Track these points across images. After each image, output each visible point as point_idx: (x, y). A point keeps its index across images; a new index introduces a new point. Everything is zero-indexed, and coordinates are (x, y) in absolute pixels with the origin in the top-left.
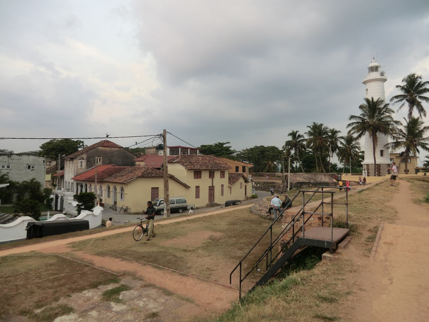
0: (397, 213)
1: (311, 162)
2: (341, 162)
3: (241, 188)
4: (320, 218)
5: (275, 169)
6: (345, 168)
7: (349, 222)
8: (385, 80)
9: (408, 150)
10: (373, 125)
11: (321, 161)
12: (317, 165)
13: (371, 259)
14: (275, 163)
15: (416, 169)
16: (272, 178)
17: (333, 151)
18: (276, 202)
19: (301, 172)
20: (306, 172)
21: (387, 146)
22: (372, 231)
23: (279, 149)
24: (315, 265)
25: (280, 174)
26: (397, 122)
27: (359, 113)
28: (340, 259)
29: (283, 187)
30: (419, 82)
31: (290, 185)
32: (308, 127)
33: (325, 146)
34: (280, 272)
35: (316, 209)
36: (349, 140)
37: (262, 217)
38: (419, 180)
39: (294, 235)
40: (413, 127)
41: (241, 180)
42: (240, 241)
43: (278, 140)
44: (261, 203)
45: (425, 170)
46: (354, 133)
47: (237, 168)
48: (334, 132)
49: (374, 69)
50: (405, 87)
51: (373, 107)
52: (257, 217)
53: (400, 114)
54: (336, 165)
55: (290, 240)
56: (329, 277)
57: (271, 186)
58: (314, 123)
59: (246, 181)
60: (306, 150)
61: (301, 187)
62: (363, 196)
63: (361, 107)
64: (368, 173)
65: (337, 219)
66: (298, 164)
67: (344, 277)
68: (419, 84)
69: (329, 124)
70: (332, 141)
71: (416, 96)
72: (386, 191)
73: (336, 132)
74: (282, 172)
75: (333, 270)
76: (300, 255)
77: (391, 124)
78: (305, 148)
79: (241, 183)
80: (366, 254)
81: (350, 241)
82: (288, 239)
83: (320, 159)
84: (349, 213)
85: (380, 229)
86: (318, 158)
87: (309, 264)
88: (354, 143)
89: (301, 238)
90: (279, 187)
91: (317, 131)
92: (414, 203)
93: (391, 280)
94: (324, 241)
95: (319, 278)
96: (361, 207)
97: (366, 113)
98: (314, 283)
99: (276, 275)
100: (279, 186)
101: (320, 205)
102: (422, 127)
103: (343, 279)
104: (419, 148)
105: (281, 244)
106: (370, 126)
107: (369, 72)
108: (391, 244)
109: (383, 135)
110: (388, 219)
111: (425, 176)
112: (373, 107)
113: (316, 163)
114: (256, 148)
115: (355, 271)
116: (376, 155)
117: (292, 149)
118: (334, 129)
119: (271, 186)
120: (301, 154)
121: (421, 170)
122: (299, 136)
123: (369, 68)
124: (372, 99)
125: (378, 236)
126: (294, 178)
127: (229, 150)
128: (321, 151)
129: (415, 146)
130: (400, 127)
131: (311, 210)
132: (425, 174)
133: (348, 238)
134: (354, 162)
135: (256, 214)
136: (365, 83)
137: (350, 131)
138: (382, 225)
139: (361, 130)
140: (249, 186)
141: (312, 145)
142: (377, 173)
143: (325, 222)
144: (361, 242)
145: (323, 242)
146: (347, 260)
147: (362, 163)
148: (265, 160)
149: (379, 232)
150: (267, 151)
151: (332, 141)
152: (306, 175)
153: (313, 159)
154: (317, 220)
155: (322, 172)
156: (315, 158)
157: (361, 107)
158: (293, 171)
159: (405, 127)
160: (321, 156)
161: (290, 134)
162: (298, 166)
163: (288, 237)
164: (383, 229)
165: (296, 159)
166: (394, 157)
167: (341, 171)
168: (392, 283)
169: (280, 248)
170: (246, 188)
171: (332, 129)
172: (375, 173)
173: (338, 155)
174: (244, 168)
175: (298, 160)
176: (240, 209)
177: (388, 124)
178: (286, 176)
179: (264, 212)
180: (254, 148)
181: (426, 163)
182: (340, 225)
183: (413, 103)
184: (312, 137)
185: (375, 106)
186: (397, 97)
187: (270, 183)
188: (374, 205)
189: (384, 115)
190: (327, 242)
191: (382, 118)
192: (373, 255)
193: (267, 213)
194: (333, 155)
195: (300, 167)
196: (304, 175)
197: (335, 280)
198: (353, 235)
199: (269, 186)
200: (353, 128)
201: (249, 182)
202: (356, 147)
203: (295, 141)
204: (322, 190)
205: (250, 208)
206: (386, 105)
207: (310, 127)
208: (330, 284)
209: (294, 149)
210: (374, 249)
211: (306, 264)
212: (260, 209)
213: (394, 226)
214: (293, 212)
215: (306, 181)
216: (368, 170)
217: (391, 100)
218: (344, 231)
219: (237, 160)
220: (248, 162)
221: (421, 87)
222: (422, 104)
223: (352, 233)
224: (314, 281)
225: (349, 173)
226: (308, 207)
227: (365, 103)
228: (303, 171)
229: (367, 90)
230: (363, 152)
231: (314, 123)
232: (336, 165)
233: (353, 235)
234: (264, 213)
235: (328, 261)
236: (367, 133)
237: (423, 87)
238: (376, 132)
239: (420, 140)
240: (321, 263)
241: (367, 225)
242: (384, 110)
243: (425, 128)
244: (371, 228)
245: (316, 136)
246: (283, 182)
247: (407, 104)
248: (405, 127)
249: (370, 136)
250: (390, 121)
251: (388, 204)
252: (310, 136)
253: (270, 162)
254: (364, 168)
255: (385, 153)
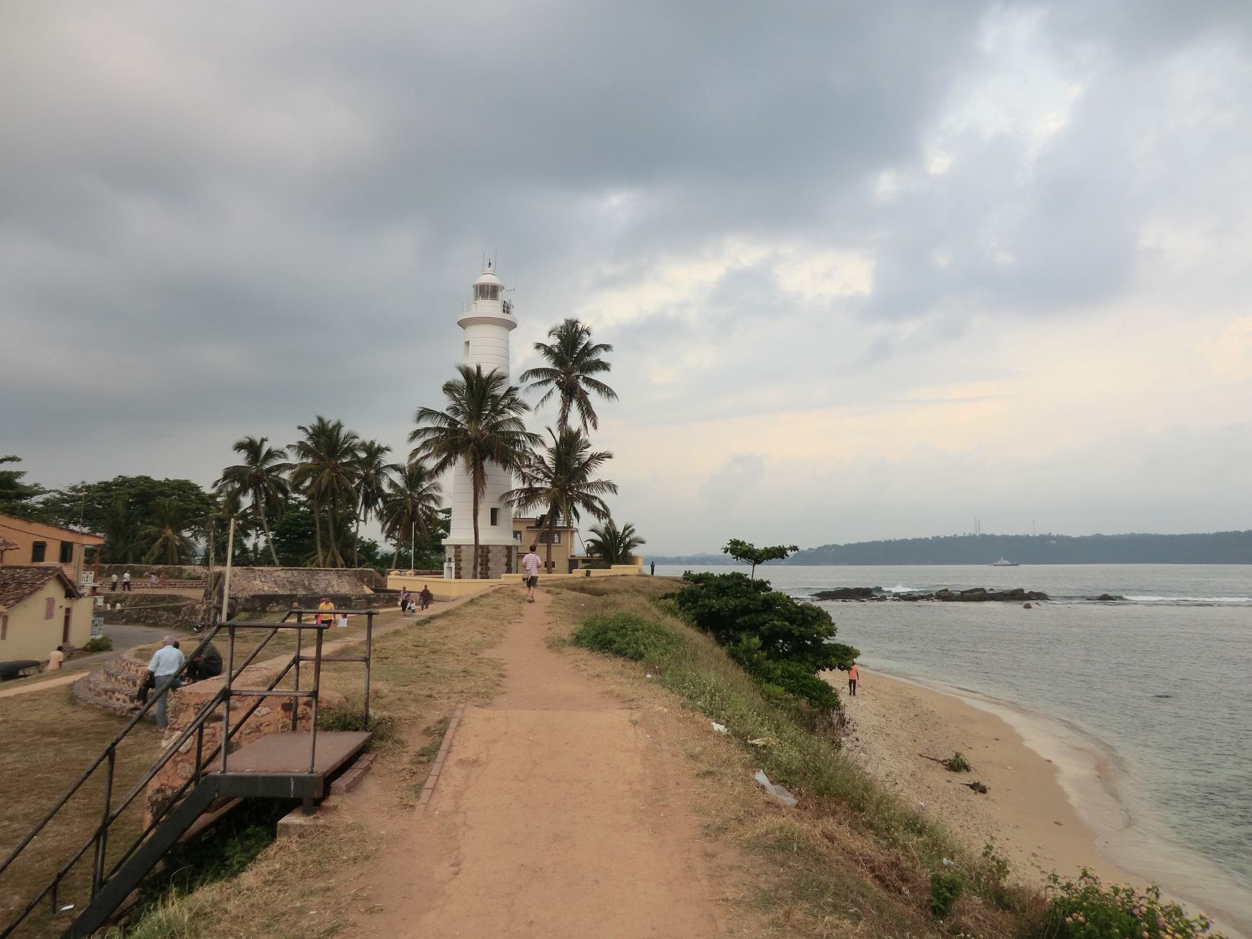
0: (504, 676)
1: (303, 535)
2: (387, 537)
3: (49, 615)
4: (286, 707)
5: (186, 555)
6: (399, 554)
7: (371, 712)
8: (511, 326)
9: (554, 513)
10: (476, 438)
11: (332, 532)
12: (319, 545)
13: (418, 814)
14: (186, 534)
15: (570, 561)
16: (172, 581)
17: (369, 503)
18: (167, 658)
19: (270, 563)
20: (285, 563)
21: (506, 497)
22: (432, 733)
23: (203, 490)
24: (252, 858)
25: (200, 570)
26: (533, 438)
27: (442, 403)
28: (329, 828)
29: (207, 611)
30: (585, 342)
31: (230, 605)
32: (300, 428)
33: (346, 490)
34: (136, 904)
35: (278, 680)
36: (415, 475)
37: (111, 714)
38: (574, 590)
39: (200, 766)
40: (568, 454)
41: (53, 590)
42: (9, 813)
43: (203, 464)
44: (113, 666)
45: (589, 563)
46: (427, 457)
47: (39, 550)
48: (374, 452)
49: (487, 291)
50: (556, 350)
51: (478, 391)
52: (93, 716)
53: (541, 416)
54: (373, 546)
55: (187, 786)
56: (286, 891)
57: (166, 609)
58: (320, 419)
59: (71, 592)
60: (287, 498)
61: (263, 611)
62: (429, 634)
63: (449, 388)
64: (458, 569)
65: (340, 706)
66: (263, 538)
67: (332, 882)
68: (586, 346)
69: (362, 427)
70: (367, 475)
71: (578, 377)
72: (492, 618)
73: (381, 450)
74: (205, 562)
75: (304, 864)
76: (213, 831)
77: (519, 441)
78: (285, 492)
79: (51, 602)
80: (405, 801)
81: (368, 769)
82: (180, 783)
83: (331, 526)
84: (376, 685)
85: (453, 724)
86: (324, 522)
87: (237, 858)
88: (425, 485)
89: (216, 777)
90: (193, 612)
91: (325, 441)
92: (550, 647)
93: (458, 864)
94: (288, 778)
95: (253, 900)
96: (416, 667)
97: (461, 405)
98: (234, 919)
99: (120, 917)
100: (193, 607)
101: (289, 666)
102: (586, 454)
103: (329, 889)
104: (579, 507)
105: (154, 803)
106: (469, 441)
107: (476, 298)
108: (475, 763)
109: (500, 468)
110: (477, 694)
111: (588, 579)
112: (478, 391)
113: (318, 538)
114: (123, 482)
115: (367, 858)
116: (479, 526)
117: (245, 492)
118: (372, 443)
119: (166, 609)
120: (273, 510)
121: (580, 564)
122: (270, 454)
123: (476, 287)
124: (479, 368)
125: (444, 746)
126: (244, 583)
127: (15, 486)
128: (334, 502)
129: (571, 501)
130: (540, 451)
131: (264, 684)
132: (588, 574)
133: (365, 760)
134: (422, 539)
135: (90, 708)
136: (463, 324)
137: (416, 451)
138: (458, 713)
139: (444, 451)
140: (83, 610)
141: (307, 483)
142: (479, 569)
143: (303, 718)
144: (399, 767)
145: (282, 781)
146: (350, 828)
147: (444, 542)
148: (151, 523)
149: (449, 735)
150: (162, 494)
151: (367, 475)
152: (281, 573)
153: (310, 525)
154: (279, 714)
155: (334, 565)
156: (314, 525)
157: (449, 388)
158: (244, 559)
159: (551, 451)
160: (334, 518)
161: (239, 447)
162: (262, 544)
163: (178, 777)
164: (459, 725)
165: (256, 524)
166: (522, 528)
167: (386, 562)
168: (457, 874)
169: (149, 817)
170: (67, 619)
171: (368, 443)
172: (475, 568)
173: (380, 515)
174: (66, 552)
175: (262, 527)
176: (31, 694)
177: (512, 439)
178: (220, 576)
179: (122, 697)
180: (116, 483)
181: (591, 544)
182: (344, 724)
183: (571, 392)
184: (310, 460)
185: (485, 391)
186: (536, 372)
187: (162, 598)
188: (451, 658)
189: (506, 416)
190: (297, 779)
191: (499, 424)
192: (425, 801)
193: (132, 700)
194: (369, 515)
195: (266, 550)
196: (275, 574)
197: (303, 896)
198: (380, 748)
199: (157, 609)
200: (425, 445)
201: (81, 596)
202: (432, 497)
203: (254, 470)
204: (299, 620)
205: (71, 686)
206: (511, 390)
207: (305, 429)
208: (283, 914)
209: (251, 492)
210: (429, 784)
211: (227, 859)
212: (109, 687)
213: (488, 712)
214: (202, 692)
215: (281, 592)
216: (458, 560)
217: (523, 378)
218: (353, 740)
219: (45, 522)
220: (86, 530)
221: (589, 355)
222: (590, 398)
223: (377, 743)
224: (234, 912)
225: (409, 568)
226: (258, 674)
227: (460, 378)
228: (277, 561)
229: (468, 343)
230: (448, 511)
231: (320, 419)
232: (373, 546)
233: (380, 748)
234: (121, 702)
235: (295, 838)
236: (461, 461)
237: (594, 358)
238: (483, 458)
239: (579, 486)
240: (272, 850)
241: (420, 717)
242: (505, 402)
243: (592, 457)
244: (431, 724)
245: (322, 458)
246: (207, 595)
247: (558, 393)
248: (551, 451)
249: (468, 469)
250: (518, 433)
251: (488, 654)
252: (304, 455)
253: (169, 532)
254: (447, 556)
255: (501, 516)
